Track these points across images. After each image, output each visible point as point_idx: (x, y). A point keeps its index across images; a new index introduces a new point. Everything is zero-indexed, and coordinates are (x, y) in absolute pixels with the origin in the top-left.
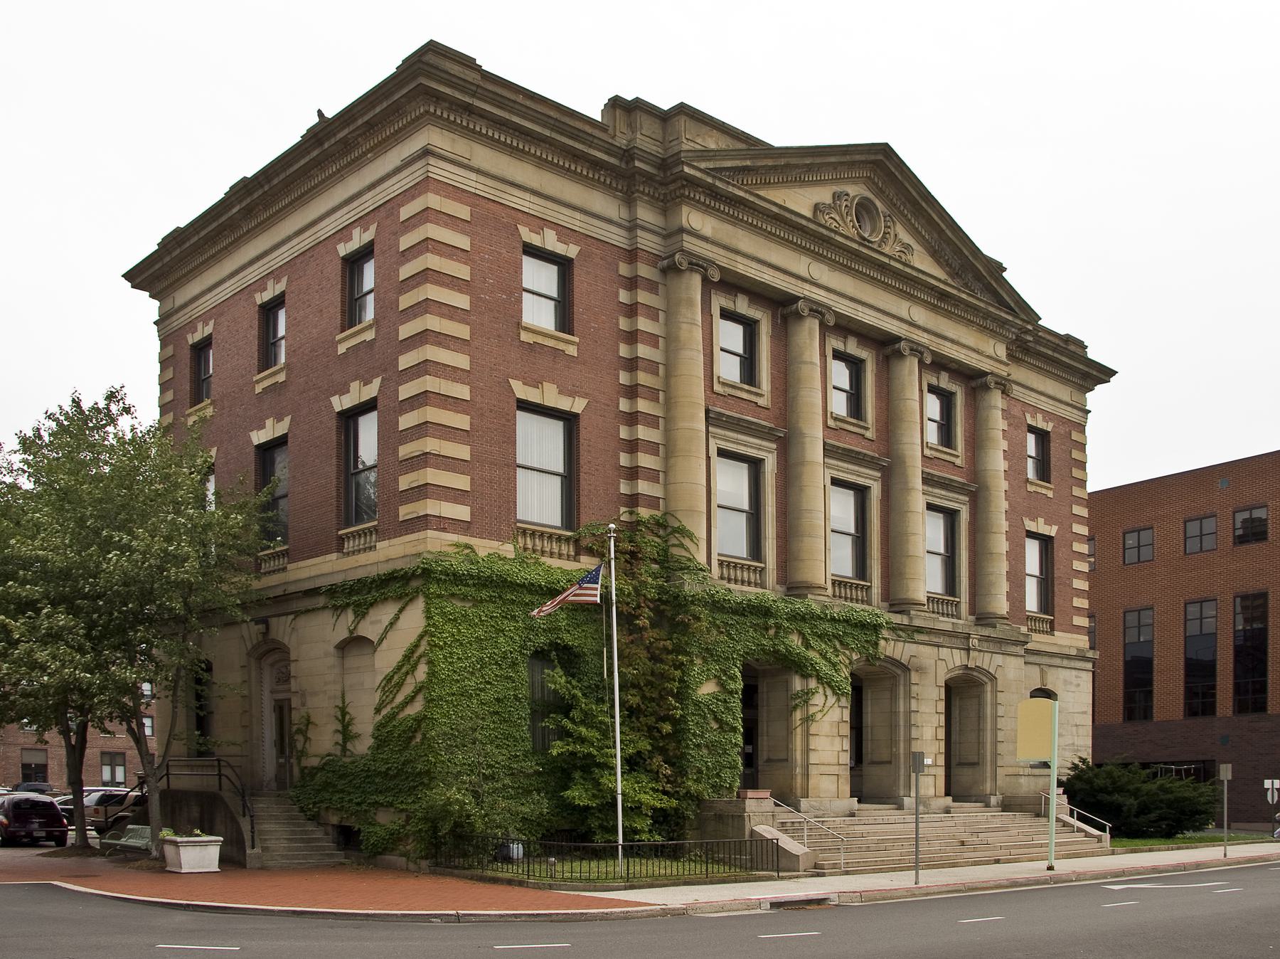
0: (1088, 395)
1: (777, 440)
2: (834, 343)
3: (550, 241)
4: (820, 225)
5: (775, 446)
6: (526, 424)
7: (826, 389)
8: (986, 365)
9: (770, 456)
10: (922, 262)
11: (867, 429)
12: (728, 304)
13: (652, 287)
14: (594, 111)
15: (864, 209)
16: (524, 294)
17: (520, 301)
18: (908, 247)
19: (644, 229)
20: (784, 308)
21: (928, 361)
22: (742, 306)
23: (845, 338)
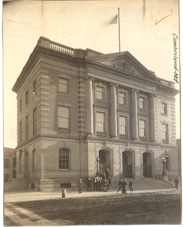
0: (175, 96)
1: (108, 109)
2: (119, 90)
3: (64, 76)
4: (115, 69)
5: (107, 110)
6: (61, 81)
7: (119, 99)
8: (151, 92)
9: (107, 112)
10: (137, 73)
11: (126, 106)
12: (121, 91)
13: (83, 83)
14: (15, 148)
15: (124, 65)
16: (59, 84)
17: (58, 118)
18: (134, 71)
19: (81, 72)
20: (109, 85)
21: (118, 86)
22: (123, 90)
23: (99, 83)
